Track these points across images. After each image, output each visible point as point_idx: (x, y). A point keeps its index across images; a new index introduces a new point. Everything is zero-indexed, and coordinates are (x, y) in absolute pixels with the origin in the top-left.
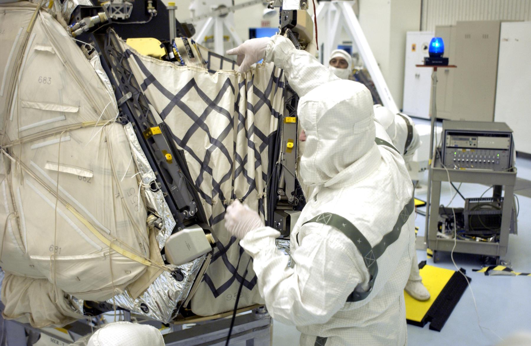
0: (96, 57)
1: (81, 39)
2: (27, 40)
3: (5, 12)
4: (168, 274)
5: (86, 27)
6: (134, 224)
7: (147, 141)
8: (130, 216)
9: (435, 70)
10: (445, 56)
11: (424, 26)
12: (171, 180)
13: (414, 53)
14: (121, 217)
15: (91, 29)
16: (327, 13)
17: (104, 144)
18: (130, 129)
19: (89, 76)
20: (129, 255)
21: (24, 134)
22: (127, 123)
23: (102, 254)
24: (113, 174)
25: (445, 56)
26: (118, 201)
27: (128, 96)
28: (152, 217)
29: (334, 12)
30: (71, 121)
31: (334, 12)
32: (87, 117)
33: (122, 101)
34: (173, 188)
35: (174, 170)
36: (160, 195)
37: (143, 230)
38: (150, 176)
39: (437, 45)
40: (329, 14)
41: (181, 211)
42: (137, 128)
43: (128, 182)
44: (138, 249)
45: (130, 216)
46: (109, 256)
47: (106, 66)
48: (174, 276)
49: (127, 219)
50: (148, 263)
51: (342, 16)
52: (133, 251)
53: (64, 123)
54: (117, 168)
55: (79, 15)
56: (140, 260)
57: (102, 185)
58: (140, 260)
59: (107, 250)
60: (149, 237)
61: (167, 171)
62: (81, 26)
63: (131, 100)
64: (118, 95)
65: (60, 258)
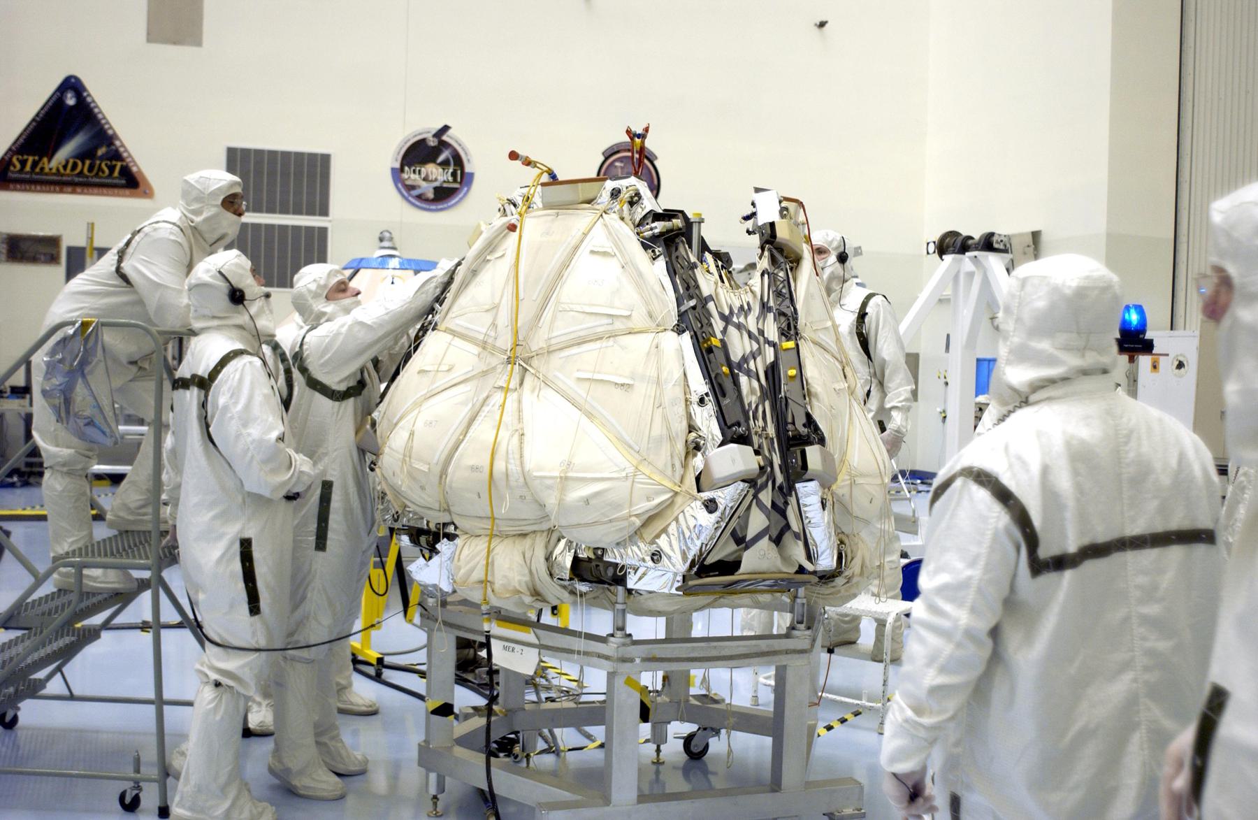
0: (661, 263)
1: (648, 244)
2: (582, 241)
3: (558, 214)
4: (699, 503)
5: (656, 231)
6: (671, 439)
7: (705, 353)
8: (669, 429)
9: (1132, 360)
10: (1148, 335)
11: (1179, 321)
12: (724, 395)
13: (1155, 375)
14: (658, 429)
15: (661, 234)
16: (956, 278)
17: (654, 350)
18: (687, 336)
19: (652, 281)
20: (657, 478)
21: (553, 341)
22: (684, 331)
23: (624, 474)
24: (658, 382)
25: (1148, 335)
26: (659, 412)
27: (692, 303)
28: (693, 435)
29: (971, 275)
30: (619, 325)
31: (971, 275)
32: (639, 320)
33: (683, 309)
34: (725, 402)
35: (728, 384)
36: (710, 407)
37: (680, 447)
38: (699, 385)
39: (1134, 318)
40: (962, 277)
41: (729, 427)
42: (695, 338)
43: (673, 392)
44: (669, 472)
45: (669, 429)
46: (631, 478)
47: (672, 272)
48: (707, 507)
49: (665, 432)
50: (677, 489)
51: (986, 283)
52: (662, 473)
53: (610, 328)
54: (664, 375)
55: (650, 220)
56: (670, 485)
57: (642, 394)
58: (670, 485)
59: (632, 469)
60: (686, 457)
61: (720, 385)
62: (651, 229)
63: (694, 308)
64: (679, 303)
65: (570, 474)
